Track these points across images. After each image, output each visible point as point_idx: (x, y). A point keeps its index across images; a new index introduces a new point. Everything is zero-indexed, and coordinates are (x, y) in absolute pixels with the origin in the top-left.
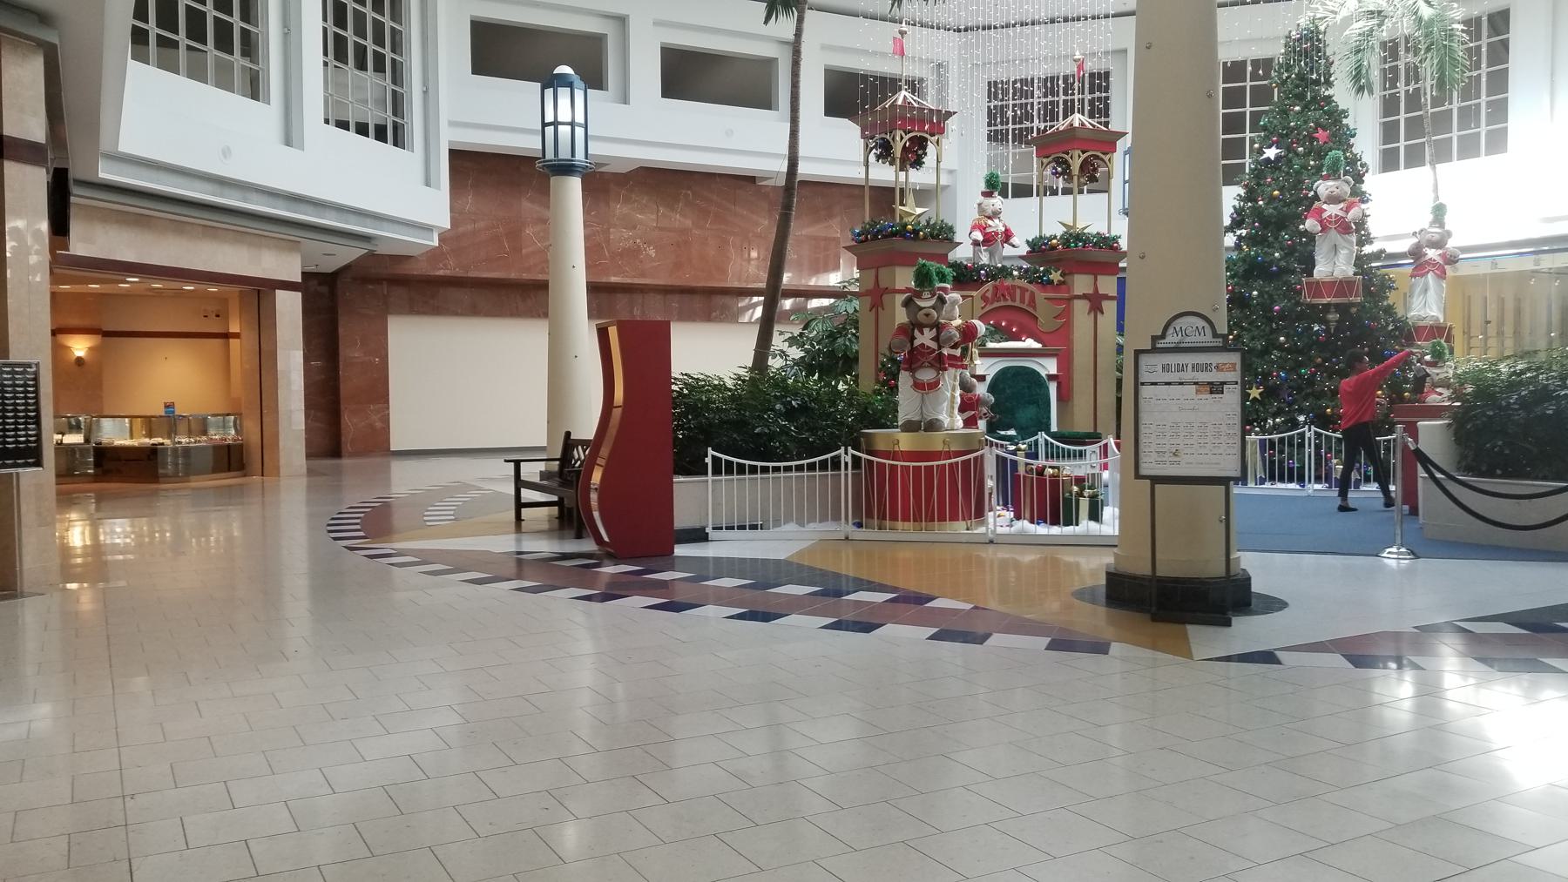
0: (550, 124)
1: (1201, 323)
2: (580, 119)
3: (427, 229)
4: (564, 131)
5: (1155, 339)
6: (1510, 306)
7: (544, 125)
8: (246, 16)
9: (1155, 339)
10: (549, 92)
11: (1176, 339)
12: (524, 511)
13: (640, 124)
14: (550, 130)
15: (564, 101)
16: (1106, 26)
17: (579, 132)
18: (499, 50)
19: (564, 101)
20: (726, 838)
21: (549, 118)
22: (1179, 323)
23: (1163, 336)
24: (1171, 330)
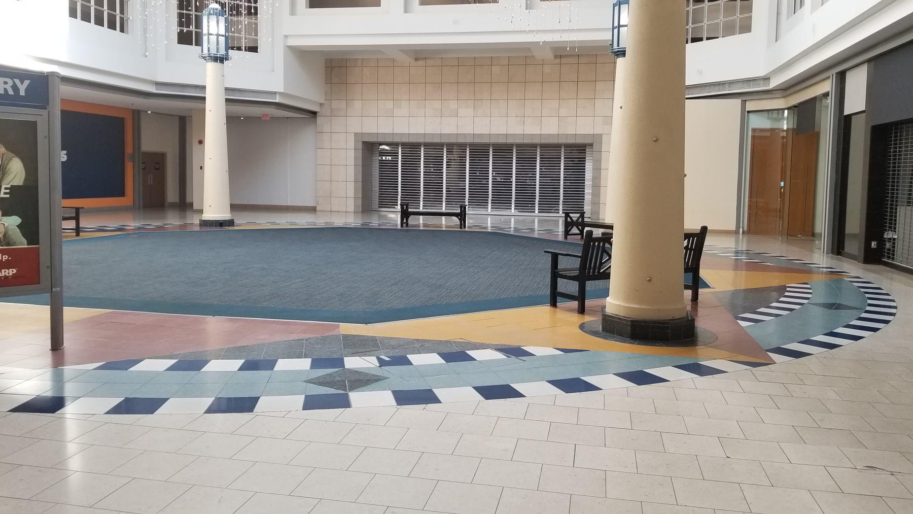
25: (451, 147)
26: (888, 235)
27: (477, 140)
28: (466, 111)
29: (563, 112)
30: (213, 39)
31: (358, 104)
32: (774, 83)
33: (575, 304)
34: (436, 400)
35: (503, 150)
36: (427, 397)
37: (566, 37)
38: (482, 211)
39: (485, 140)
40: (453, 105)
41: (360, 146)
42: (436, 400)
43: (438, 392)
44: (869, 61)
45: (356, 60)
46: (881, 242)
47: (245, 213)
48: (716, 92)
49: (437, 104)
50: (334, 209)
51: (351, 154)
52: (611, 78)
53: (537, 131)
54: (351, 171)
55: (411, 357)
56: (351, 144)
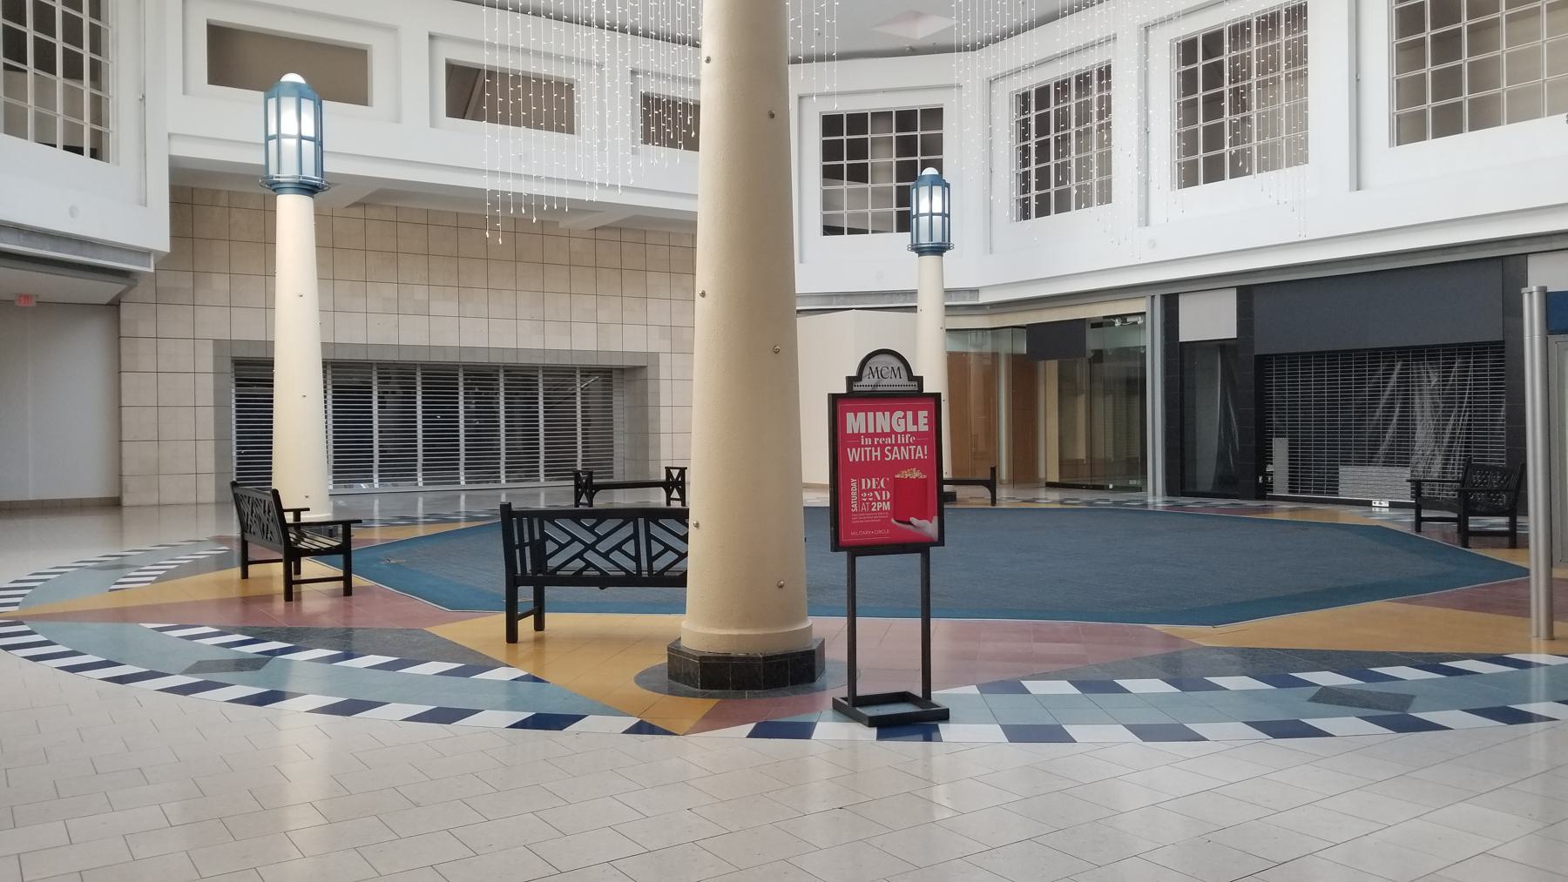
0: (273, 138)
1: (896, 364)
2: (309, 130)
3: (144, 253)
4: (290, 144)
5: (850, 380)
6: (526, 626)
7: (268, 138)
8: (96, 12)
9: (850, 380)
10: (272, 102)
11: (873, 381)
12: (251, 568)
13: (400, 135)
14: (273, 144)
15: (289, 114)
16: (602, 38)
17: (308, 147)
18: (233, 57)
19: (289, 114)
20: (554, 871)
21: (273, 131)
22: (873, 363)
23: (859, 377)
24: (866, 371)
25: (588, 372)
26: (1269, 469)
27: (438, 358)
28: (444, 306)
29: (603, 316)
30: (290, 144)
31: (220, 283)
32: (984, 298)
33: (1506, 540)
34: (1069, 739)
35: (482, 377)
36: (1056, 734)
37: (525, 188)
38: (404, 487)
39: (452, 358)
40: (420, 293)
41: (228, 366)
42: (1069, 739)
43: (1070, 729)
44: (1239, 288)
45: (218, 191)
46: (1266, 475)
47: (19, 522)
48: (833, 303)
49: (390, 291)
50: (165, 499)
51: (207, 383)
52: (267, 241)
53: (564, 345)
54: (207, 417)
55: (1027, 684)
56: (206, 361)
